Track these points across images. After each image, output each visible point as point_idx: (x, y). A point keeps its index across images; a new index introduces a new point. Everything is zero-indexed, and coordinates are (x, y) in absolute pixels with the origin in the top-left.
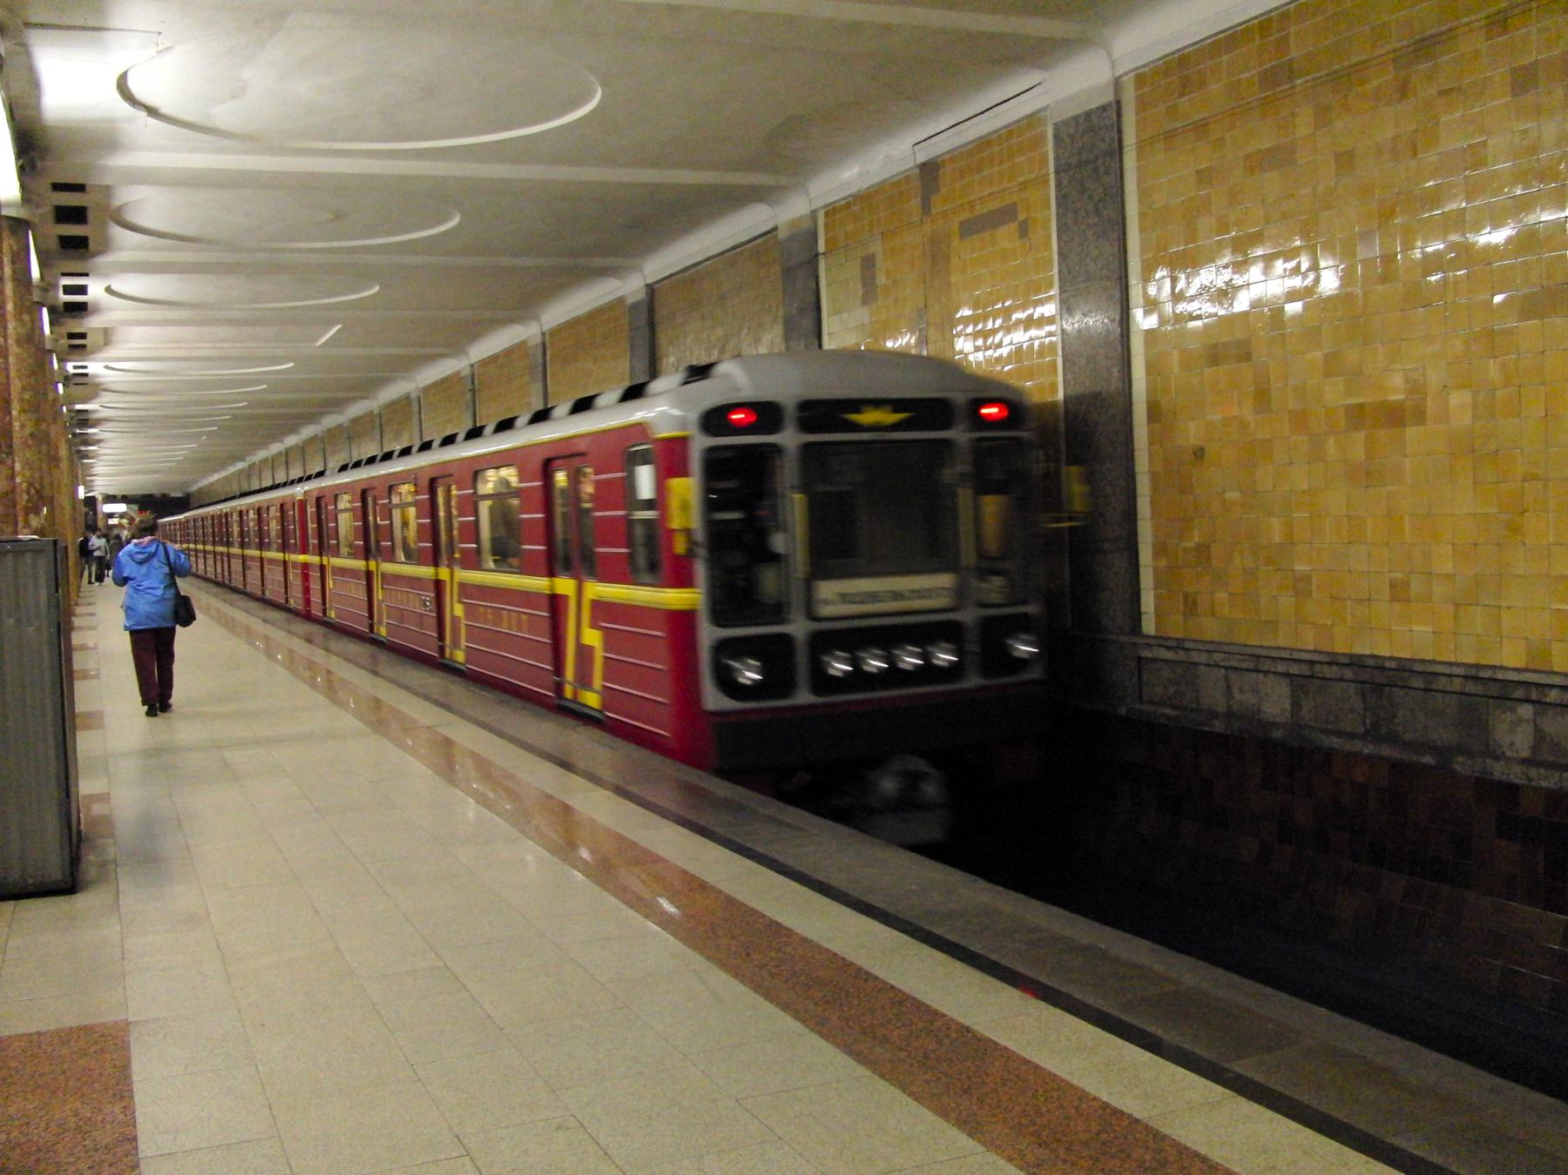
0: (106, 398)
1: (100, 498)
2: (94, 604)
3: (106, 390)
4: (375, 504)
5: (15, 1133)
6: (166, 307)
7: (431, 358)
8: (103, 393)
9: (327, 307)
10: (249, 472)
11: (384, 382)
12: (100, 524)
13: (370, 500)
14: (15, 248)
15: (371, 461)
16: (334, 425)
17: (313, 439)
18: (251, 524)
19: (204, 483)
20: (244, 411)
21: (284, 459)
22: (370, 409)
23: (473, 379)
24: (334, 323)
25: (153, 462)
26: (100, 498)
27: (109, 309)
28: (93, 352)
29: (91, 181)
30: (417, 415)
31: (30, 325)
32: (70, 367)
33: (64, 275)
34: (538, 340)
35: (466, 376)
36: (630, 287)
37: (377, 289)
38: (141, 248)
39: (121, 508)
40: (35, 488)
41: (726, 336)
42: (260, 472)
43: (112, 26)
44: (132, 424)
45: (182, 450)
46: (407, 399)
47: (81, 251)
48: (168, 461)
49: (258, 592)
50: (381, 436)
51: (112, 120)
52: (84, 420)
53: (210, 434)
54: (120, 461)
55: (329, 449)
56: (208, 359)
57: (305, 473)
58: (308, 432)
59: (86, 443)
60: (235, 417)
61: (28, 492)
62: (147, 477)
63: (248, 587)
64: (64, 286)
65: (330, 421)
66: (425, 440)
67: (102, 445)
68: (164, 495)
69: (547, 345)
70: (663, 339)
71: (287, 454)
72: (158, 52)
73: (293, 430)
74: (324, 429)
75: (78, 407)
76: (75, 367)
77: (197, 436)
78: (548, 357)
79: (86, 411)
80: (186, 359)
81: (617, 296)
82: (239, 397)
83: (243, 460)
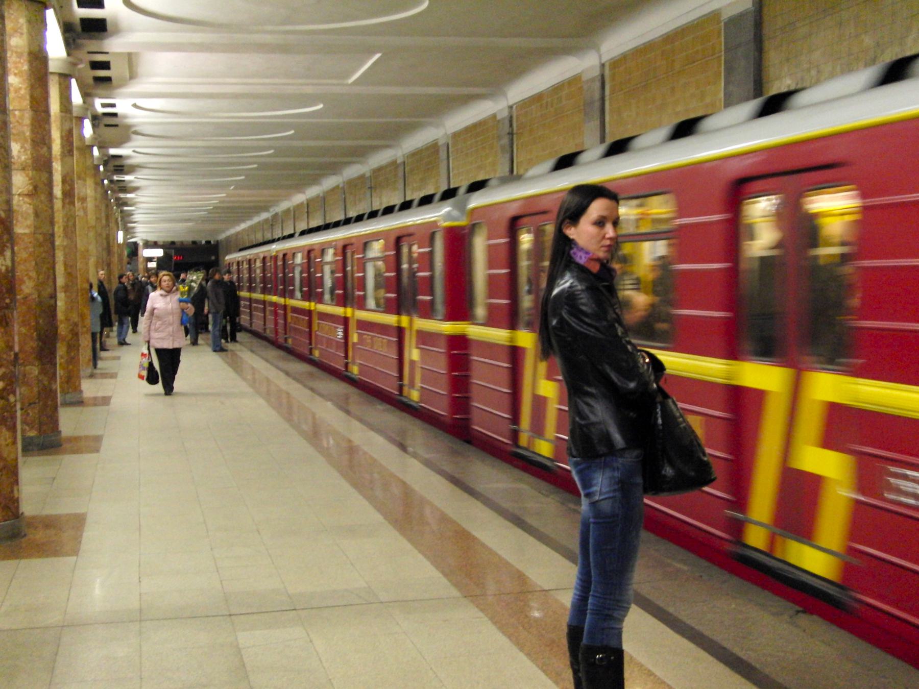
1: (141, 243)
4: (352, 256)
7: (466, 100)
8: (134, 137)
9: (365, 30)
10: (272, 223)
11: (411, 128)
13: (349, 255)
15: (389, 210)
16: (356, 175)
17: (334, 190)
18: (258, 271)
19: (232, 231)
20: (268, 160)
22: (394, 158)
24: (372, 52)
26: (141, 243)
28: (120, 86)
30: (445, 162)
32: (98, 105)
34: (596, 73)
35: (503, 119)
39: (159, 253)
41: (878, 44)
44: (162, 172)
46: (433, 148)
49: (260, 330)
52: (118, 166)
54: (157, 209)
57: (282, 235)
58: (330, 182)
62: (181, 224)
63: (253, 325)
65: (353, 171)
66: (348, 217)
67: (139, 193)
68: (194, 243)
71: (308, 204)
73: (315, 180)
74: (345, 180)
75: (113, 151)
76: (104, 106)
77: (222, 186)
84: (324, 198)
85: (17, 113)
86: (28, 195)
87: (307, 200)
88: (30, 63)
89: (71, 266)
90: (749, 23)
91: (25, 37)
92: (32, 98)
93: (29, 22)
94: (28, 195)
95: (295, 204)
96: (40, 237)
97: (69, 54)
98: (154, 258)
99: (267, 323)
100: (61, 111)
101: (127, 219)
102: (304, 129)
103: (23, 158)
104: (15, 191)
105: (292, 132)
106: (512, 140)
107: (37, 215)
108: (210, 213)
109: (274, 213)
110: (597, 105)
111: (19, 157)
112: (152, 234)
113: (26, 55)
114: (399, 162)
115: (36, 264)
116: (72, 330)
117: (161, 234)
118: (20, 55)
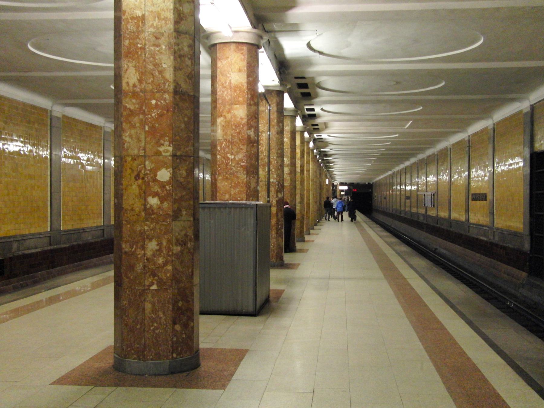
0: (331, 147)
2: (323, 225)
3: (330, 144)
5: (207, 369)
6: (340, 115)
12: (338, 194)
14: (278, 101)
19: (378, 179)
21: (404, 171)
23: (469, 142)
24: (409, 120)
25: (357, 171)
27: (324, 116)
29: (306, 76)
31: (282, 127)
33: (305, 105)
34: (492, 127)
36: (524, 106)
37: (421, 108)
38: (329, 96)
39: (346, 188)
40: (281, 184)
42: (396, 176)
43: (301, 29)
45: (367, 166)
46: (446, 149)
47: (309, 97)
48: (362, 170)
50: (437, 163)
51: (307, 57)
53: (375, 161)
55: (420, 168)
56: (366, 133)
58: (413, 160)
59: (329, 163)
60: (382, 154)
61: (278, 185)
64: (306, 109)
65: (421, 156)
69: (495, 129)
70: (536, 128)
72: (317, 36)
73: (407, 159)
75: (322, 150)
76: (317, 136)
78: (495, 134)
79: (326, 151)
80: (358, 133)
81: (519, 110)
82: (381, 147)
83: (391, 170)
84: (411, 167)
85: (286, 149)
86: (289, 174)
87: (405, 167)
88: (291, 134)
89: (302, 195)
90: (529, 115)
91: (290, 126)
92: (291, 145)
93: (291, 122)
94: (289, 174)
95: (401, 168)
96: (292, 187)
97: (304, 125)
98: (344, 190)
99: (495, 237)
100: (301, 143)
101: (331, 173)
102: (394, 142)
103: (288, 163)
104: (285, 173)
105: (390, 143)
106: (469, 148)
107: (291, 180)
108: (366, 171)
109: (393, 172)
110: (492, 138)
111: (286, 163)
112: (343, 180)
113: (290, 132)
114: (448, 148)
115: (291, 195)
116: (302, 216)
117: (346, 180)
118: (288, 132)
